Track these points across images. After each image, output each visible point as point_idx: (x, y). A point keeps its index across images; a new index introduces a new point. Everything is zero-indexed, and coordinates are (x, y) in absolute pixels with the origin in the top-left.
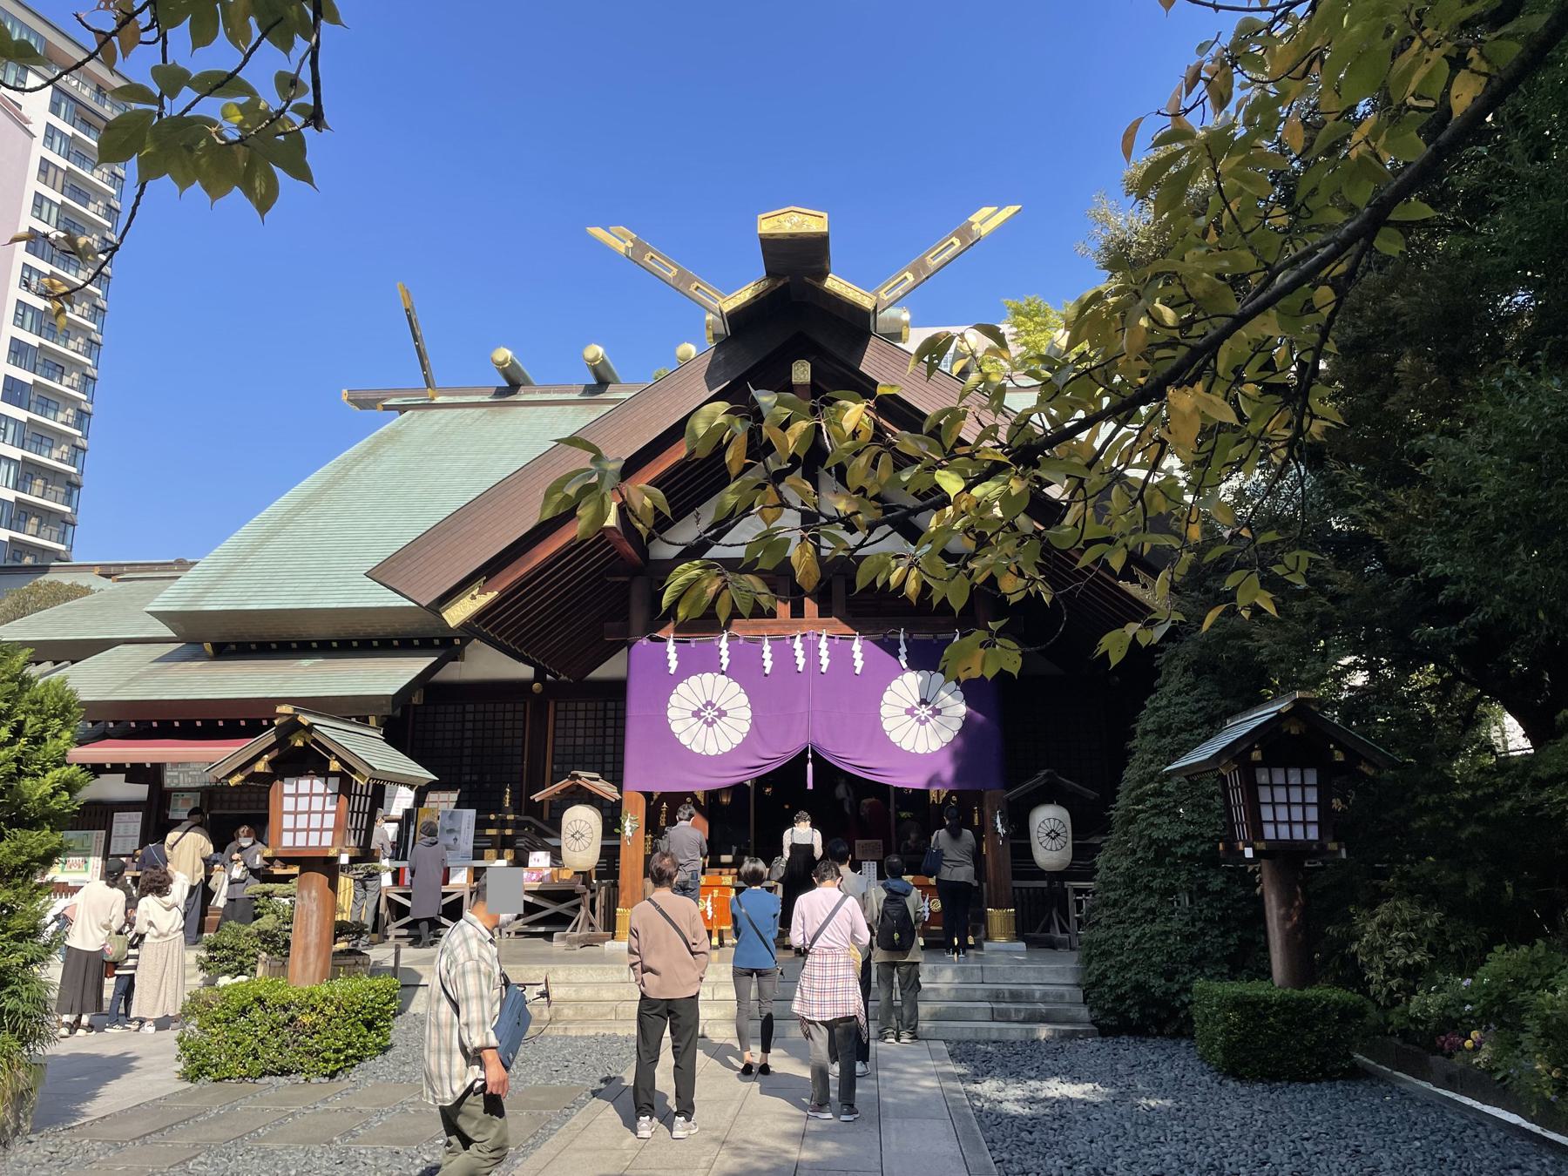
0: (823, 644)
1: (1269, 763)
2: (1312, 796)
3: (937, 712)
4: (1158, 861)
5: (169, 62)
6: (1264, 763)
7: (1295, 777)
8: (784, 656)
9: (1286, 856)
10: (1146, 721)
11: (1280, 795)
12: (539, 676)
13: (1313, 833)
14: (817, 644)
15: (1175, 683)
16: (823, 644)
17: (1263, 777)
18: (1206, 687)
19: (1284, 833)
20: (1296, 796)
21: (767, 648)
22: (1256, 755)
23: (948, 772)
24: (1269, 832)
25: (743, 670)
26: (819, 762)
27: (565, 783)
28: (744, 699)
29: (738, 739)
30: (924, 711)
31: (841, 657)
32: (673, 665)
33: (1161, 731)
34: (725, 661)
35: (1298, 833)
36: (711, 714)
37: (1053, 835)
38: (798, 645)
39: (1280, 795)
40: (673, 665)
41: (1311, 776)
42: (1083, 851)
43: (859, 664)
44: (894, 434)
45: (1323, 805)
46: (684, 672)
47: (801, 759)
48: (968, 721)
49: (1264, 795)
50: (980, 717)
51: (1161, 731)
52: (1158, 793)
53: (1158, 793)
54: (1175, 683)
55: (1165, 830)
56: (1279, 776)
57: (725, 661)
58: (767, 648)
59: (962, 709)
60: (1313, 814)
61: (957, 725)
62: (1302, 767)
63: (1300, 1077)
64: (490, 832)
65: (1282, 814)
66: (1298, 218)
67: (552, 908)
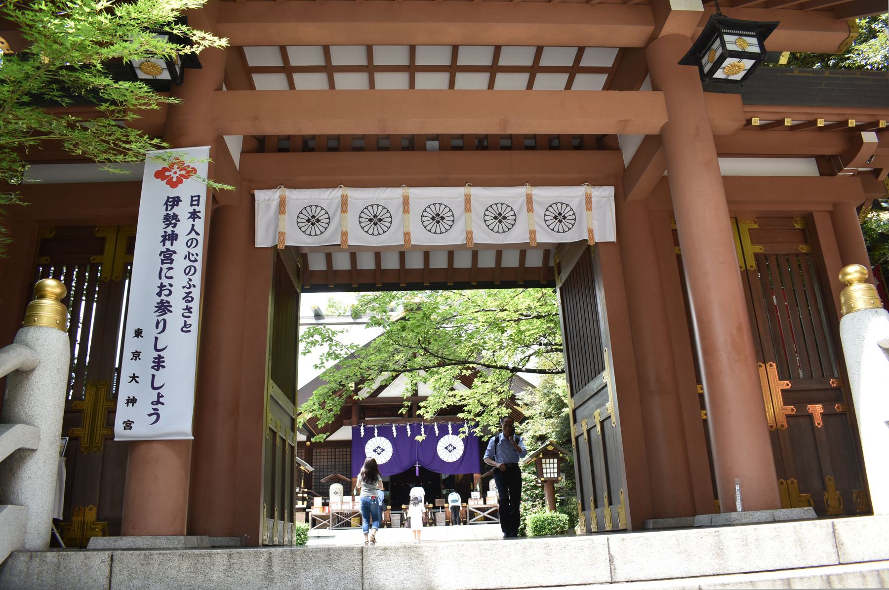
1: (545, 457)
7: (551, 460)
11: (548, 466)
12: (309, 439)
13: (556, 475)
17: (543, 461)
22: (541, 456)
39: (548, 466)
41: (556, 461)
56: (548, 461)
62: (553, 458)
65: (548, 471)
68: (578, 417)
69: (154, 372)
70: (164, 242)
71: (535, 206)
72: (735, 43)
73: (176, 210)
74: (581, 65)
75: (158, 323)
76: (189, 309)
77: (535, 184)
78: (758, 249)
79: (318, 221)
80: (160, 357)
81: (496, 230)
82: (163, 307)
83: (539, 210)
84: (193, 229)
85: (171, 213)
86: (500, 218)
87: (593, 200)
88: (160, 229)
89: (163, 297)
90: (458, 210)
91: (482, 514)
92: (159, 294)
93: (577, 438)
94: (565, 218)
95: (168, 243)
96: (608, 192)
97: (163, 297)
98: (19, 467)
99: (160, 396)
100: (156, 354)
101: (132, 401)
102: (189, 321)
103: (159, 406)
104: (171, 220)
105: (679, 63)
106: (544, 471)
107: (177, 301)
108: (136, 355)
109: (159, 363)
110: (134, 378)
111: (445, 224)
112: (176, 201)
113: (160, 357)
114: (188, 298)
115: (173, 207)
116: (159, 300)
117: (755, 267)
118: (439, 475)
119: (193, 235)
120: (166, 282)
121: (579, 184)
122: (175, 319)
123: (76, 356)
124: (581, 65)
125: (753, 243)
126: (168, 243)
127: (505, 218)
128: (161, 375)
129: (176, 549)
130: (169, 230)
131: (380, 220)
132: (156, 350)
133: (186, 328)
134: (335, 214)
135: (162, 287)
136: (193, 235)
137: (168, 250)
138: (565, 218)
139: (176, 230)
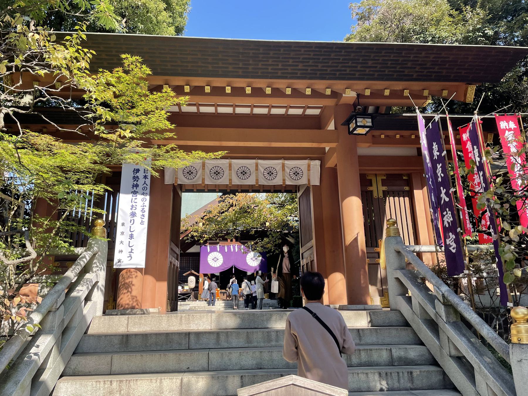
0: (236, 247)
8: (229, 248)
14: (235, 247)
16: (236, 247)
21: (226, 247)
25: (222, 251)
26: (235, 268)
27: (189, 272)
28: (222, 257)
32: (209, 250)
34: (218, 250)
36: (215, 259)
38: (232, 247)
40: (209, 250)
46: (211, 252)
47: (232, 267)
57: (218, 250)
58: (226, 247)
64: (353, 208)
67: (183, 297)
69: (130, 240)
70: (133, 187)
71: (286, 168)
72: (361, 122)
73: (138, 174)
75: (131, 221)
76: (143, 215)
78: (385, 188)
79: (192, 173)
80: (132, 234)
82: (133, 215)
83: (287, 170)
84: (145, 183)
85: (136, 175)
86: (270, 173)
87: (311, 166)
88: (132, 182)
89: (133, 210)
90: (253, 169)
91: (183, 297)
92: (132, 209)
94: (298, 174)
95: (135, 188)
96: (318, 163)
97: (133, 210)
98: (458, 330)
99: (132, 250)
100: (130, 233)
101: (122, 251)
102: (143, 220)
103: (131, 254)
104: (136, 178)
105: (342, 125)
107: (139, 212)
108: (122, 233)
109: (131, 237)
110: (122, 242)
111: (247, 175)
112: (138, 171)
113: (132, 234)
114: (143, 211)
115: (136, 173)
116: (131, 211)
117: (382, 196)
118: (246, 273)
119: (145, 185)
120: (134, 204)
121: (305, 158)
122: (138, 219)
125: (382, 186)
126: (135, 188)
127: (272, 174)
128: (132, 242)
130: (135, 183)
131: (219, 173)
132: (130, 231)
133: (142, 223)
134: (199, 170)
135: (132, 206)
137: (135, 191)
138: (298, 174)
139: (138, 183)
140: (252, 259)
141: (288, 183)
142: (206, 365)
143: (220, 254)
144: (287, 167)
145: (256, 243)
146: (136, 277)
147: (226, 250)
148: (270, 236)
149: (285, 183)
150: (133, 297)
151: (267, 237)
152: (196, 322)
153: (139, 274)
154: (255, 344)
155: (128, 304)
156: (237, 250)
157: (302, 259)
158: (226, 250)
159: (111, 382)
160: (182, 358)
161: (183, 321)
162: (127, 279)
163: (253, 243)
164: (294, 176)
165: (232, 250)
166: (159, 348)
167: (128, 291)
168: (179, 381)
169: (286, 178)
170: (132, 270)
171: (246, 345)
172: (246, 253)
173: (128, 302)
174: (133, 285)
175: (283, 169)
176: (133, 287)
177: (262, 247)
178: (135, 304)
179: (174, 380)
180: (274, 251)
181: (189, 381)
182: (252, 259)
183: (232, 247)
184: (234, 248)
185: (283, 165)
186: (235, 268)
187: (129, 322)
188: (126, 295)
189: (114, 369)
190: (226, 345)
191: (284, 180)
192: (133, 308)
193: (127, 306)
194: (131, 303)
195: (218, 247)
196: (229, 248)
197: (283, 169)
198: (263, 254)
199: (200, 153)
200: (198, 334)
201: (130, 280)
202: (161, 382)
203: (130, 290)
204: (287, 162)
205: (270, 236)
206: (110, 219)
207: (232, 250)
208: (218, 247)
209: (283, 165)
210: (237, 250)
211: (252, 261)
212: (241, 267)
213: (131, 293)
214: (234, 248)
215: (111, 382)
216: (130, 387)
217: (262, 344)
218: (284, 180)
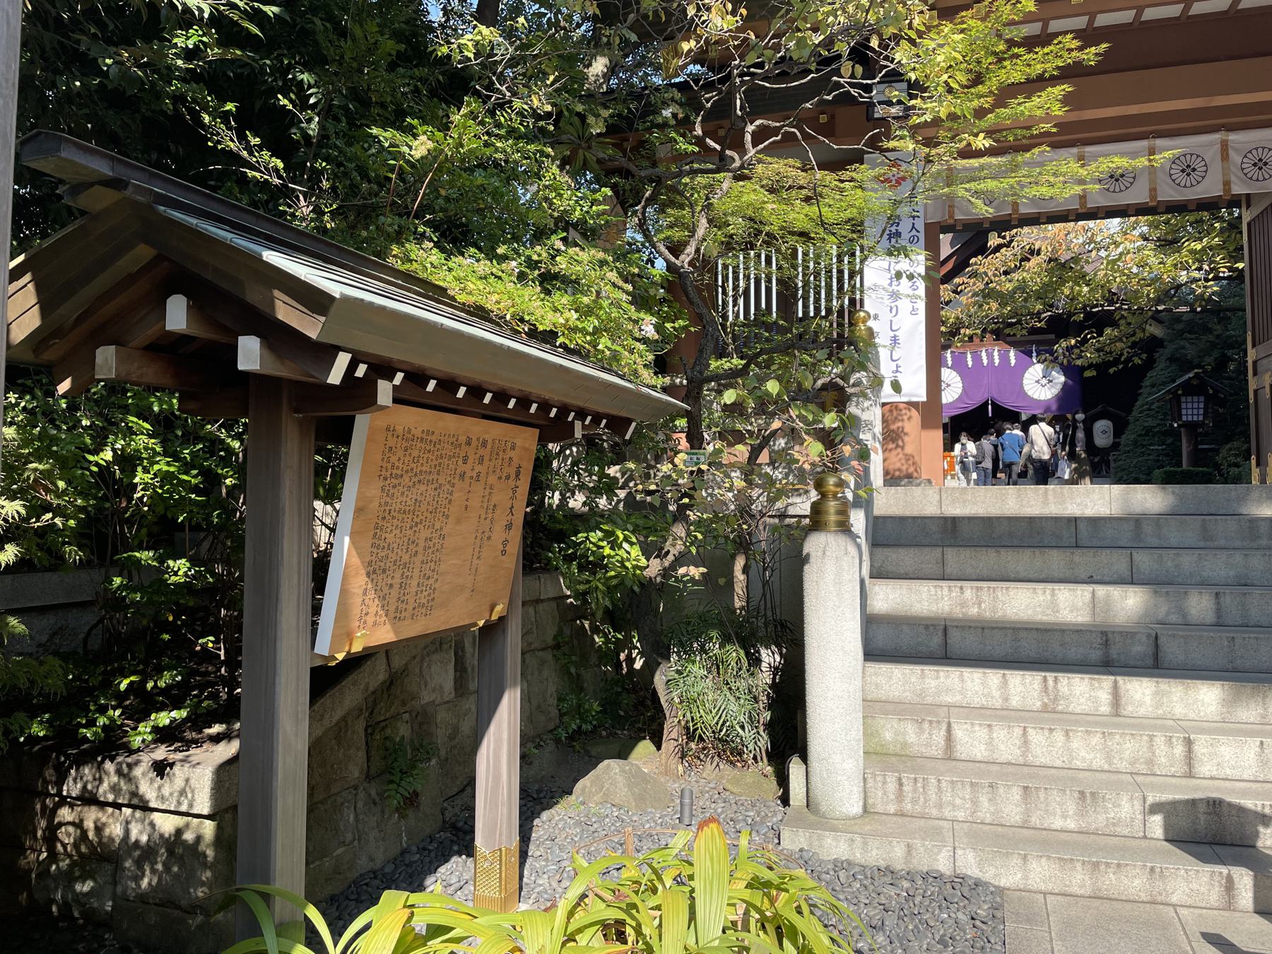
0: (996, 353)
1: (1185, 394)
2: (1202, 405)
3: (1050, 381)
4: (1146, 435)
5: (1018, 731)
6: (1183, 395)
8: (977, 358)
9: (1191, 427)
10: (1147, 382)
11: (1190, 405)
13: (1201, 418)
14: (993, 354)
15: (1162, 365)
16: (996, 353)
17: (1183, 399)
18: (1174, 367)
19: (1190, 418)
20: (1195, 405)
21: (969, 356)
23: (1054, 407)
24: (1184, 418)
26: (993, 404)
28: (958, 379)
29: (956, 396)
30: (1044, 381)
31: (1004, 358)
33: (1153, 386)
34: (950, 363)
35: (1195, 418)
37: (1104, 432)
38: (984, 354)
39: (1190, 405)
41: (1202, 399)
42: (1117, 433)
43: (1013, 362)
44: (315, 300)
45: (1205, 409)
47: (986, 403)
48: (1065, 384)
49: (1183, 406)
50: (1070, 382)
51: (1153, 386)
52: (1149, 409)
53: (1149, 409)
54: (1162, 365)
55: (1151, 422)
56: (1189, 399)
57: (950, 363)
58: (969, 356)
59: (1062, 379)
60: (1201, 411)
61: (1059, 387)
63: (1137, 481)
65: (1190, 412)
66: (109, 396)
68: (1259, 370)
71: (1231, 152)
74: (1040, 24)
77: (1231, 128)
81: (1188, 184)
83: (1236, 158)
93: (1256, 392)
95: (893, 240)
100: (892, 334)
106: (1184, 412)
119: (914, 232)
123: (800, 303)
124: (1040, 24)
127: (1194, 170)
129: (1190, 942)
130: (893, 229)
133: (914, 312)
136: (914, 232)
140: (1037, 382)
141: (1238, 189)
142: (1127, 573)
143: (954, 373)
144: (1236, 150)
145: (1085, 341)
146: (910, 418)
147: (970, 363)
148: (1122, 322)
149: (1230, 189)
150: (908, 457)
151: (1114, 324)
152: (1079, 501)
153: (914, 412)
154: (1222, 542)
155: (899, 470)
156: (997, 361)
157: (1255, 374)
158: (970, 363)
159: (961, 588)
160: (1077, 559)
161: (1051, 498)
162: (894, 423)
163: (1073, 342)
164: (1254, 172)
165: (985, 362)
166: (1016, 542)
167: (897, 446)
168: (1088, 596)
169: (1233, 178)
170: (902, 406)
171: (1202, 544)
172: (1022, 369)
173: (898, 465)
174: (906, 434)
175: (1225, 156)
176: (906, 439)
177: (1098, 350)
178: (911, 470)
179: (1079, 592)
180: (1129, 359)
181: (1108, 596)
182: (1037, 382)
183: (984, 354)
184: (990, 356)
185: (1225, 146)
186: (993, 404)
187: (944, 497)
188: (894, 453)
189: (948, 570)
190: (1154, 542)
191: (1227, 184)
192: (909, 476)
193: (897, 473)
194: (904, 468)
195: (949, 355)
196: (977, 358)
197: (1225, 156)
198: (1067, 370)
199: (1116, 159)
200: (1095, 522)
201: (900, 424)
202: (1053, 595)
203: (900, 443)
204: (1233, 137)
205: (1122, 322)
206: (763, 306)
207: (985, 362)
208: (949, 355)
209: (1225, 146)
210: (997, 361)
211: (1040, 384)
212: (1008, 402)
213: (903, 448)
214: (990, 356)
215: (961, 588)
216: (995, 599)
217: (1238, 543)
218: (1227, 184)
